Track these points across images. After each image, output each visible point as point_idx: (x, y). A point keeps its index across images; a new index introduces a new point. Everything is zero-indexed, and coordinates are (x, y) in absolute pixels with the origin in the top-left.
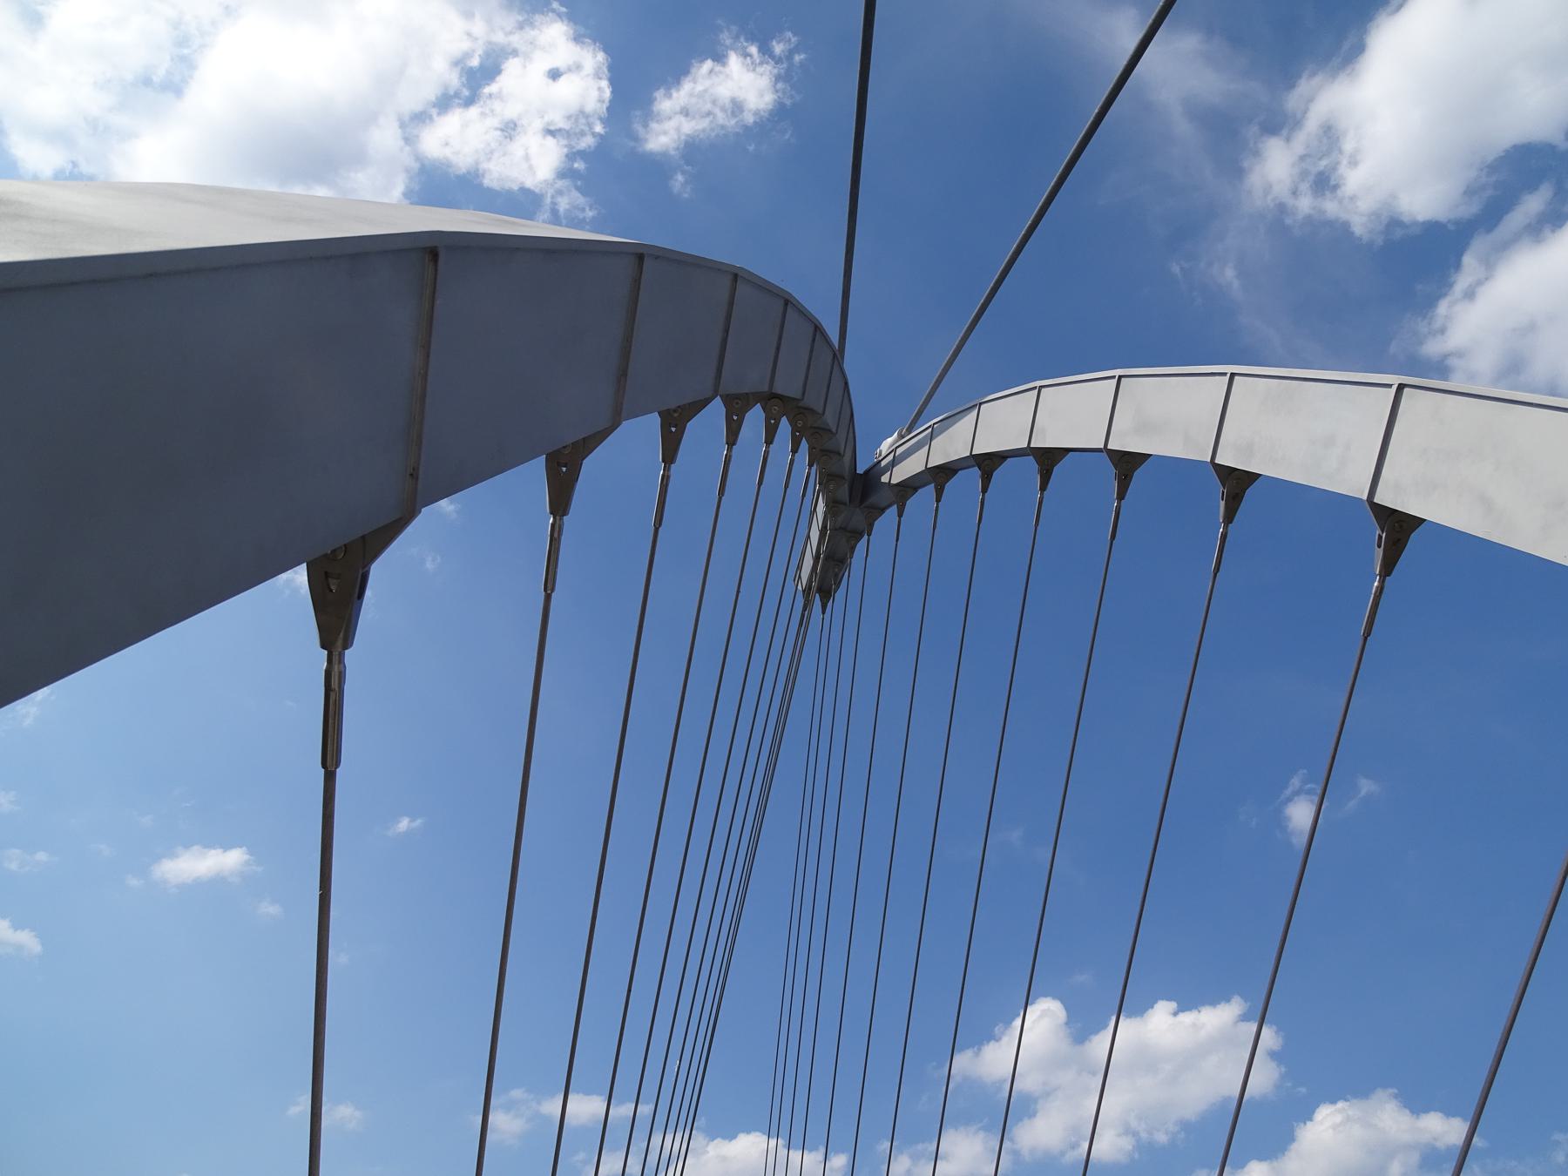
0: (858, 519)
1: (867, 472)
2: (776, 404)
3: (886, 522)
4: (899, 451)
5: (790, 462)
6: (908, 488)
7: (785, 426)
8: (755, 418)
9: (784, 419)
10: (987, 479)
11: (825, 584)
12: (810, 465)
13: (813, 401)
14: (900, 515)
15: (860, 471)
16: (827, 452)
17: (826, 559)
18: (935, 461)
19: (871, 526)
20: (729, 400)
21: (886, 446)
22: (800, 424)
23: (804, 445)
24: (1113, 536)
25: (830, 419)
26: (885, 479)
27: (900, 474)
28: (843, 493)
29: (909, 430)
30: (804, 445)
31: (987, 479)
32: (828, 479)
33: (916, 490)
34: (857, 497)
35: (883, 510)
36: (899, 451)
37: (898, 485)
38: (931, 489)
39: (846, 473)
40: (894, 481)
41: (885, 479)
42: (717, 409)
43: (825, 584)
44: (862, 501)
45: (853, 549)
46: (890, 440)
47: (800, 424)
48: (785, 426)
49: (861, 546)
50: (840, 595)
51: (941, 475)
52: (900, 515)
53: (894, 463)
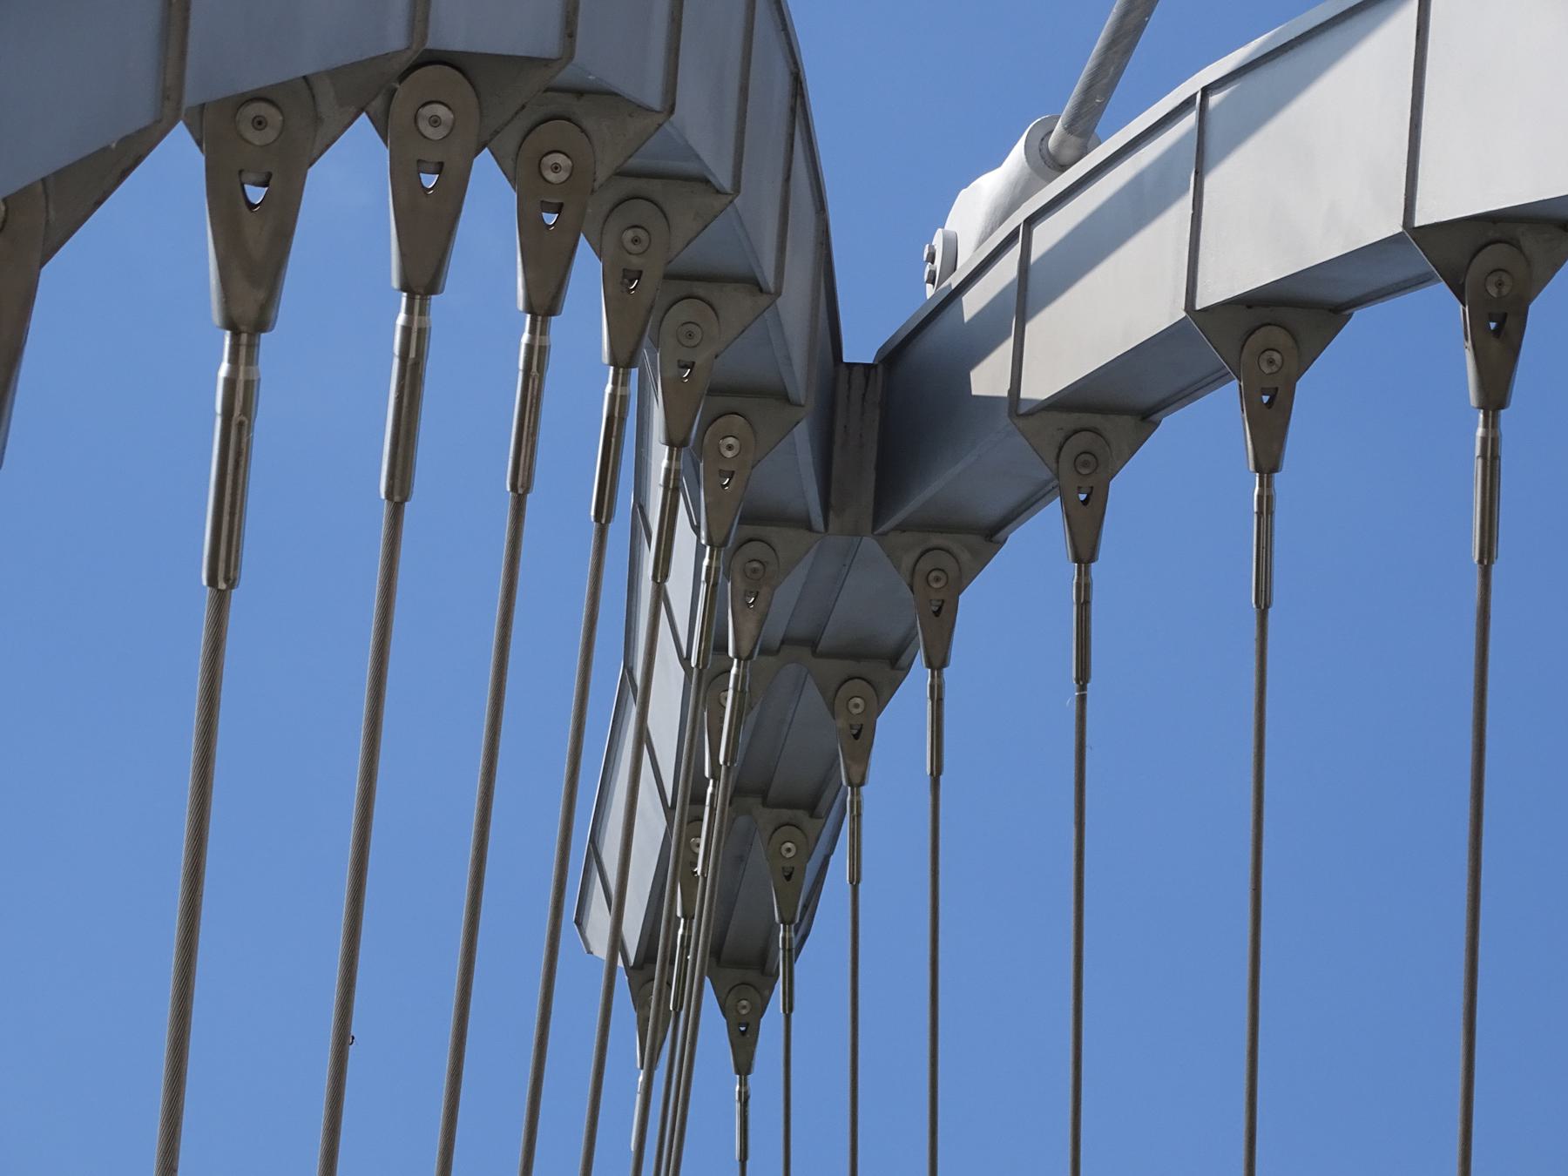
0: (872, 589)
1: (895, 354)
2: (438, 98)
3: (1017, 590)
4: (1046, 236)
5: (525, 352)
6: (1107, 417)
7: (490, 201)
8: (350, 182)
9: (485, 167)
10: (1498, 336)
11: (730, 942)
12: (623, 360)
13: (618, 56)
14: (1084, 552)
15: (860, 347)
16: (692, 282)
17: (737, 793)
18: (1234, 272)
19: (941, 616)
20: (218, 127)
21: (972, 214)
22: (557, 169)
23: (587, 272)
24: (1083, 676)
25: (700, 130)
26: (989, 378)
27: (1065, 348)
28: (791, 472)
29: (1084, 127)
30: (587, 272)
31: (1498, 336)
32: (715, 409)
33: (1146, 418)
34: (871, 486)
35: (992, 535)
36: (1046, 236)
37: (1063, 403)
38: (1219, 415)
39: (799, 377)
40: (1039, 386)
41: (989, 378)
42: (178, 160)
43: (730, 942)
44: (884, 502)
45: (860, 737)
46: (989, 187)
47: (557, 169)
48: (490, 201)
49: (902, 719)
50: (818, 964)
51: (1270, 336)
52: (1084, 552)
53: (1024, 300)
